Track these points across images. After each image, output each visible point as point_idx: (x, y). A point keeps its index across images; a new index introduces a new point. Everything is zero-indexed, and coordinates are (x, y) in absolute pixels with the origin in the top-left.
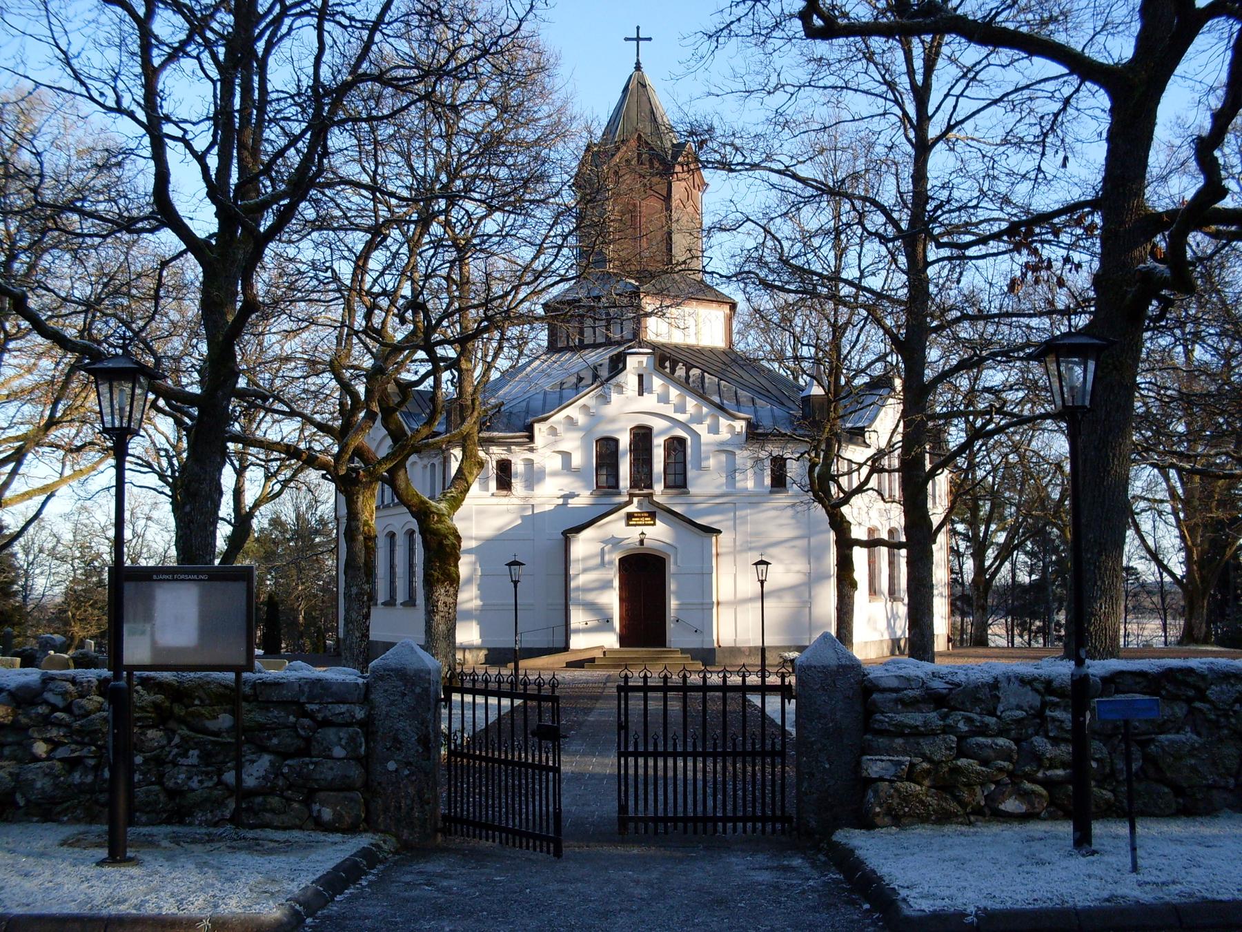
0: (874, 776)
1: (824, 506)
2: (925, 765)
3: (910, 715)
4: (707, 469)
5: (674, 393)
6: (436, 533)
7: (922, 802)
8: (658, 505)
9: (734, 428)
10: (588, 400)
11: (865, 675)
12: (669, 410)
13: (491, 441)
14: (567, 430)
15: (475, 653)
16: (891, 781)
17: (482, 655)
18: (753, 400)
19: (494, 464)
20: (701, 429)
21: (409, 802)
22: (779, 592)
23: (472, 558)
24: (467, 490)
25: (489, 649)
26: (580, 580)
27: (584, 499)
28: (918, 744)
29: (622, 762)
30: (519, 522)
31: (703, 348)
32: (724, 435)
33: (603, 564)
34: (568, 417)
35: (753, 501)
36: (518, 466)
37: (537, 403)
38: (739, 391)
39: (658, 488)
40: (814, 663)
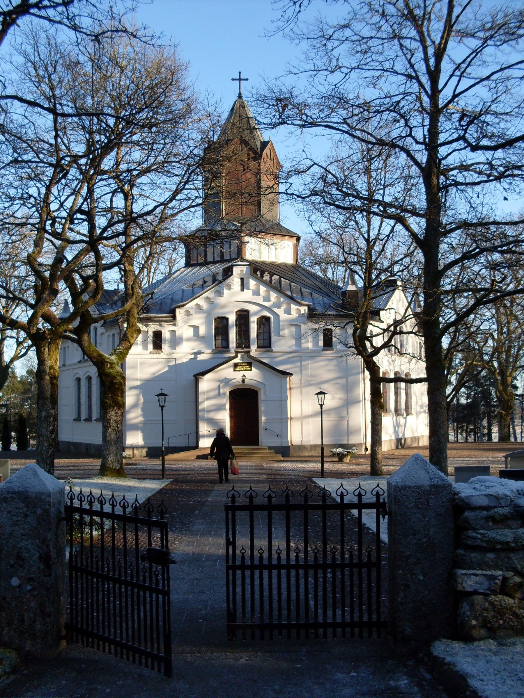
0: (469, 589)
1: (362, 356)
2: (517, 579)
3: (500, 531)
4: (283, 336)
5: (263, 289)
6: (108, 375)
7: (515, 614)
8: (253, 358)
9: (300, 310)
10: (210, 294)
11: (455, 494)
12: (260, 301)
13: (150, 320)
14: (196, 313)
15: (140, 450)
16: (486, 595)
17: (144, 451)
18: (311, 294)
19: (152, 335)
20: (280, 311)
21: (31, 615)
22: (330, 410)
23: (135, 392)
24: (130, 348)
25: (149, 448)
26: (204, 405)
27: (206, 355)
28: (509, 558)
29: (230, 516)
30: (167, 369)
31: (280, 264)
32: (294, 315)
33: (219, 395)
34: (197, 304)
35: (312, 355)
36: (166, 335)
37: (178, 297)
38: (303, 289)
39: (253, 348)
40: (409, 484)
